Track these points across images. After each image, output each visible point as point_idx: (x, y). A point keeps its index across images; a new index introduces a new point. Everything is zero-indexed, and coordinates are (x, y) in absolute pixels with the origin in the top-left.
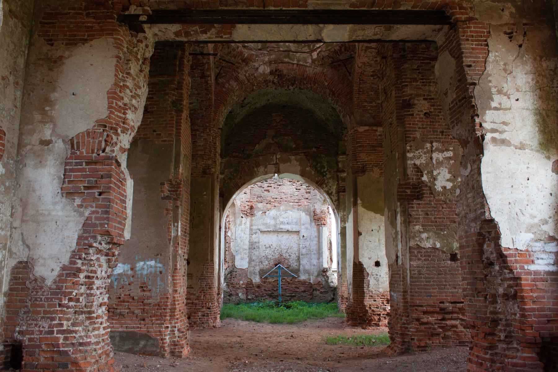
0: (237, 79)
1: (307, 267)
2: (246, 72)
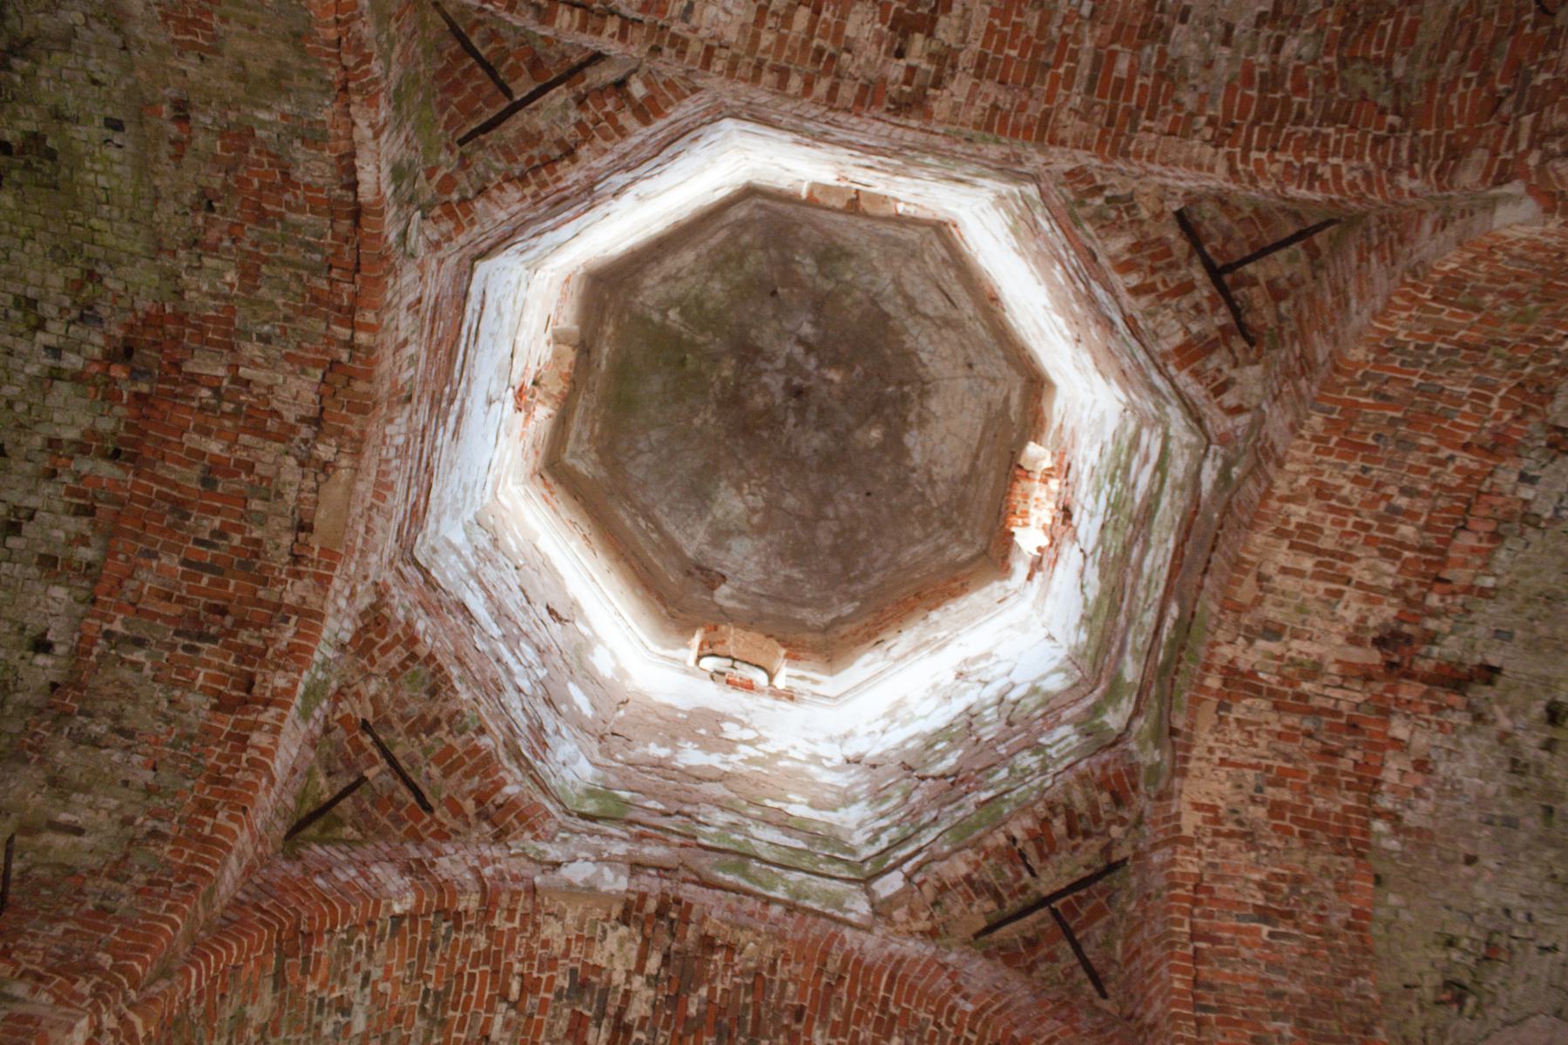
2: (485, 862)
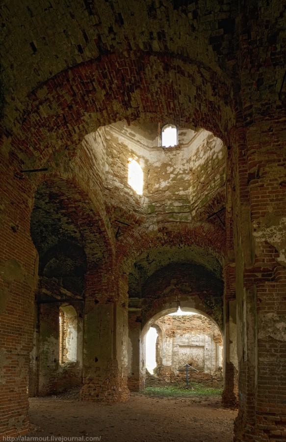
0: (132, 236)
1: (209, 366)
2: (139, 230)
